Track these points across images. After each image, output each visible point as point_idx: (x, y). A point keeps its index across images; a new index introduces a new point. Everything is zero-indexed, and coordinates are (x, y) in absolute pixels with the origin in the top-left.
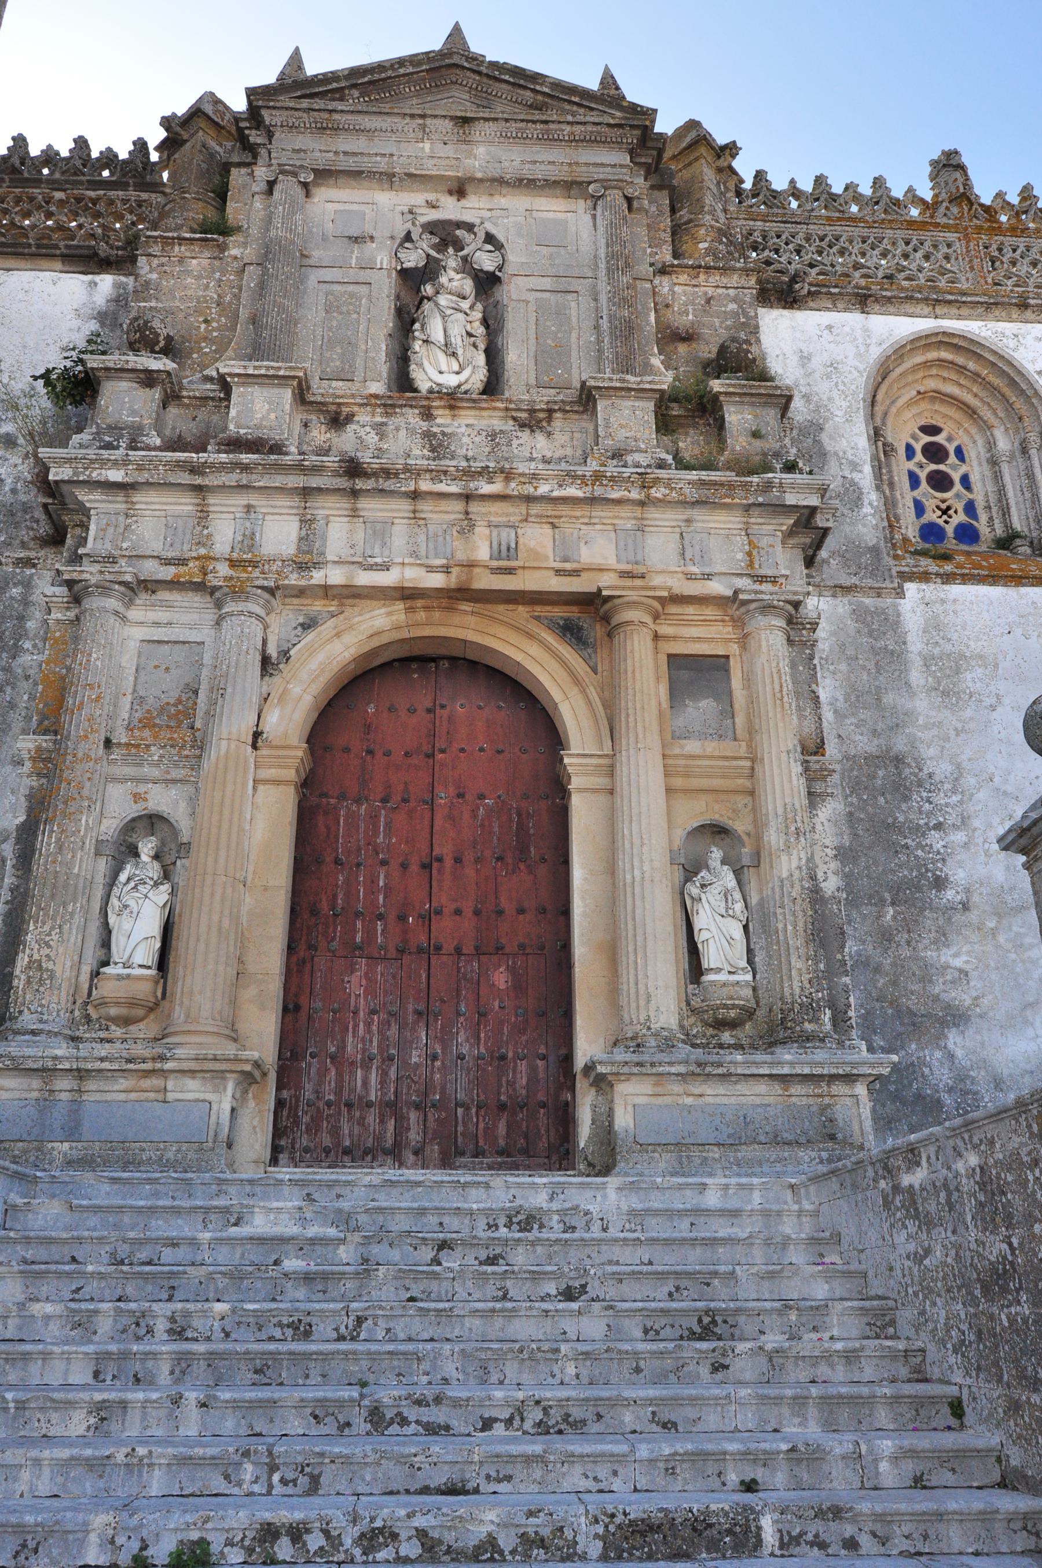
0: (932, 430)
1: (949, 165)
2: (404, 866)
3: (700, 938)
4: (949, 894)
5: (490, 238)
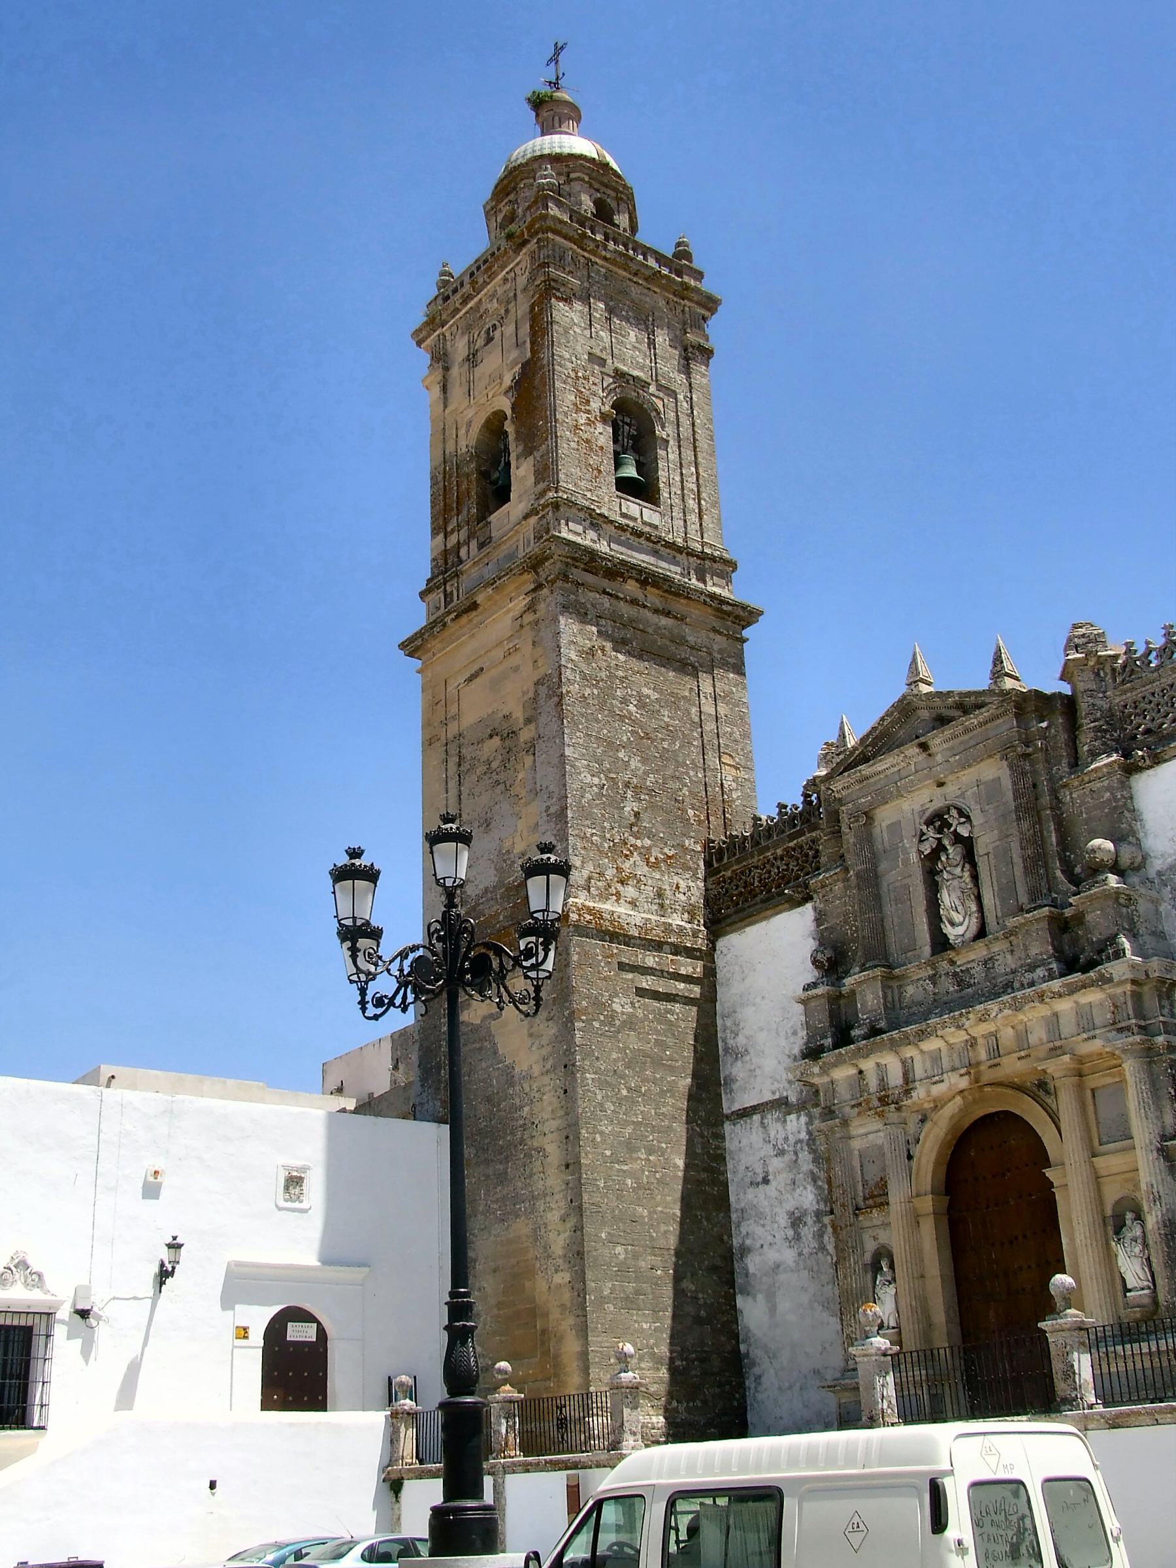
2: (1002, 1244)
3: (899, 1305)
5: (961, 813)
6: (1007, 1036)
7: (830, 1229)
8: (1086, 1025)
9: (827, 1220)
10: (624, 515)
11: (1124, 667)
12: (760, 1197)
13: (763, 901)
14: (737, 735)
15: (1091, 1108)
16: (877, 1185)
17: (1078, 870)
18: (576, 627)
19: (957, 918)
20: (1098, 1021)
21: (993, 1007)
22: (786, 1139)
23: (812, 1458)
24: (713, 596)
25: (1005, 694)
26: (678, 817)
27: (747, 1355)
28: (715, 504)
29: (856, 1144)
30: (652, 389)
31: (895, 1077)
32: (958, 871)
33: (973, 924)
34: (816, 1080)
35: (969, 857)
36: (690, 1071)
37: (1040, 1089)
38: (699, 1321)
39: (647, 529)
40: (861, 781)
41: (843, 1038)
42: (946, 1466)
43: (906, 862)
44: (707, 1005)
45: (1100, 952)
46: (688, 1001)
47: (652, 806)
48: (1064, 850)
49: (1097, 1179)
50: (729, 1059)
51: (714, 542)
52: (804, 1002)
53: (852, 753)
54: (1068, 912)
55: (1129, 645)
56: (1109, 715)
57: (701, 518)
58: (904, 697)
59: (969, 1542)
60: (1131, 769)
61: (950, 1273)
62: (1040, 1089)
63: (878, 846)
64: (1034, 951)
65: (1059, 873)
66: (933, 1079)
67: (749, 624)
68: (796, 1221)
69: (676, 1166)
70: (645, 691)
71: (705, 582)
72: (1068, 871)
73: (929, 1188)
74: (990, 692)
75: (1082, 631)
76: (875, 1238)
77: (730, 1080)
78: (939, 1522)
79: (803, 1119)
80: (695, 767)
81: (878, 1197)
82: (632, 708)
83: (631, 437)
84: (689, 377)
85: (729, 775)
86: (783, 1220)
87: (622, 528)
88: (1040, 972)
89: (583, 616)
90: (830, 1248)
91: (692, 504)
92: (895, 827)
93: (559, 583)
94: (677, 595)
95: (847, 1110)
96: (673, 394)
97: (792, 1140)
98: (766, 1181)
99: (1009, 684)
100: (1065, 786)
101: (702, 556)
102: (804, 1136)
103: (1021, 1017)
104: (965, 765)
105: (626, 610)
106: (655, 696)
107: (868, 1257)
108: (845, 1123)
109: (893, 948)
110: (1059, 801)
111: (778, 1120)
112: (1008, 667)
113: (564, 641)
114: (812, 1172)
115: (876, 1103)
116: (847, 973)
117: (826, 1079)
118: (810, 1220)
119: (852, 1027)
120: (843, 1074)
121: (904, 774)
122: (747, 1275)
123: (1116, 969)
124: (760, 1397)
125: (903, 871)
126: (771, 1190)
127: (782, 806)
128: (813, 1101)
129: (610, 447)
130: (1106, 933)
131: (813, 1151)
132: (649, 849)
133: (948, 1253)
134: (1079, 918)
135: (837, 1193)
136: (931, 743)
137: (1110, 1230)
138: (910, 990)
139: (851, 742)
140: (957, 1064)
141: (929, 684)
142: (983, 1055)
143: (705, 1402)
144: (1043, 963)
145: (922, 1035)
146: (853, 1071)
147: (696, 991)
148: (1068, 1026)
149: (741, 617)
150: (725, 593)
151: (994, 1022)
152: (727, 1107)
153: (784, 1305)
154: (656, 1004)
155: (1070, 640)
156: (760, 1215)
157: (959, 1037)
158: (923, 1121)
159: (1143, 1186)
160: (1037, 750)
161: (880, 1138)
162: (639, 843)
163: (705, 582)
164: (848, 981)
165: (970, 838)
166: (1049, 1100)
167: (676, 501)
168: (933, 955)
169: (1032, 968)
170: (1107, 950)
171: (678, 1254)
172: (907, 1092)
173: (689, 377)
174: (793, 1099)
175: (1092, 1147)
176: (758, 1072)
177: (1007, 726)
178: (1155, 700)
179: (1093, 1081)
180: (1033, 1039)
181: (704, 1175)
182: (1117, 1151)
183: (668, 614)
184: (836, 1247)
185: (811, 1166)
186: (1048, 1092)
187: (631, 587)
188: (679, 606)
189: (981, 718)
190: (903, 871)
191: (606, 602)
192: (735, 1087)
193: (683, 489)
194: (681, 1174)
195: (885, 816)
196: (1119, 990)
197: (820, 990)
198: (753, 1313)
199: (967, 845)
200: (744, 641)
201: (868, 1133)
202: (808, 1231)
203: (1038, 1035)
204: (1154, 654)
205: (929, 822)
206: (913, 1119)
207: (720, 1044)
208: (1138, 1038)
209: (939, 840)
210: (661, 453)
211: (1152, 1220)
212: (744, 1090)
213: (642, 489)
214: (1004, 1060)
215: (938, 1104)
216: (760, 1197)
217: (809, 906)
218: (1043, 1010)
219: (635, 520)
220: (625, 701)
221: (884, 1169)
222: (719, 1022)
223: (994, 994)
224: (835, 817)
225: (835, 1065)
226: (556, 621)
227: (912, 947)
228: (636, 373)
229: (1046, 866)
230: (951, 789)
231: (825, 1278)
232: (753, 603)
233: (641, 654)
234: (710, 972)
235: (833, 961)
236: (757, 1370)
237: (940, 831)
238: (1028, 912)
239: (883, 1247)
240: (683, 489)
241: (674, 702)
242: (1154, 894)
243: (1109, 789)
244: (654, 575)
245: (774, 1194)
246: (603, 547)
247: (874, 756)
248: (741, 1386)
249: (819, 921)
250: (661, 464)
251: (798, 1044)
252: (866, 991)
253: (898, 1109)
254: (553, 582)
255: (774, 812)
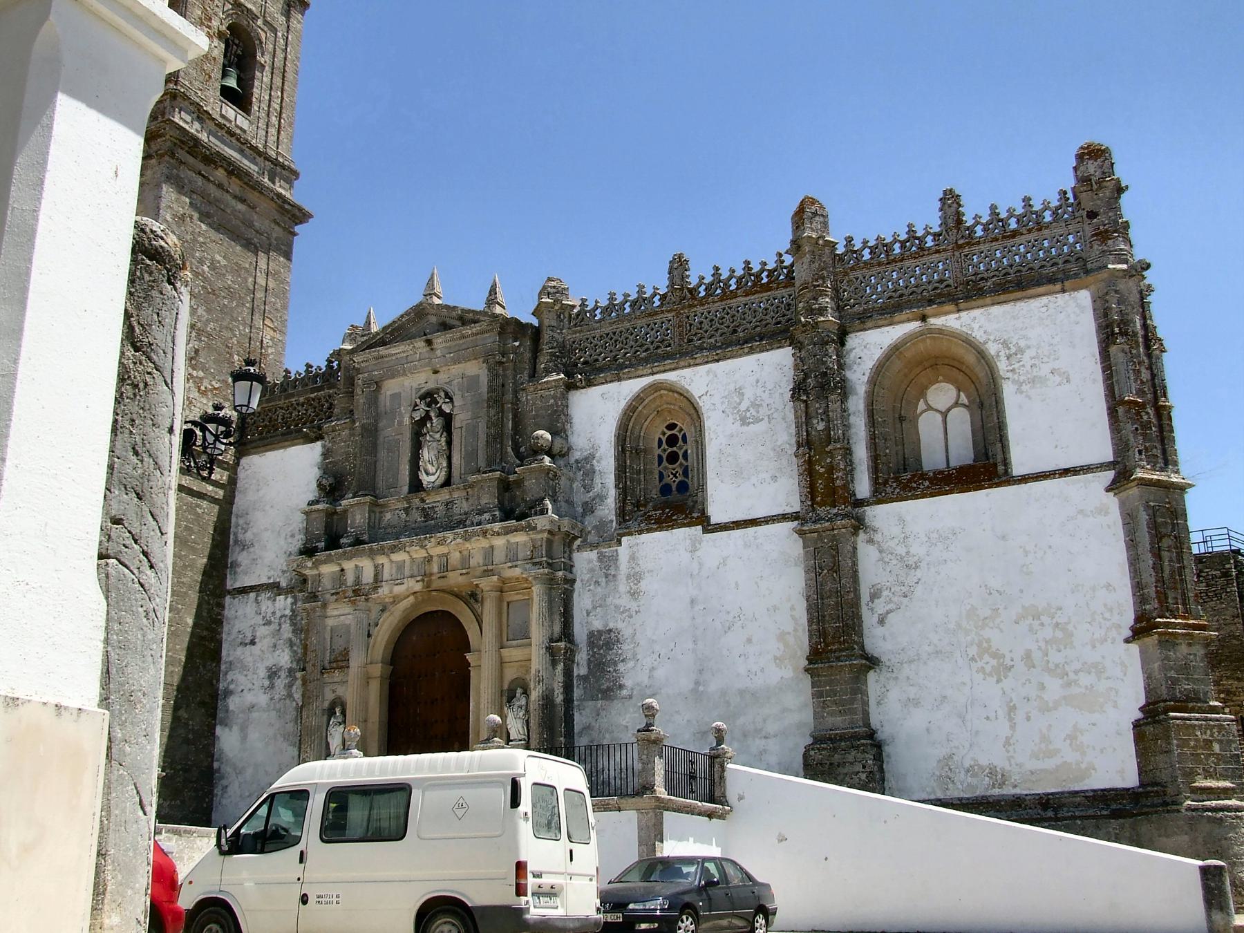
0: (672, 427)
1: (950, 200)
4: (624, 692)
5: (447, 396)
6: (455, 557)
7: (299, 682)
8: (512, 557)
9: (299, 675)
10: (222, 116)
11: (578, 314)
12: (247, 655)
13: (283, 434)
14: (278, 306)
15: (505, 615)
16: (340, 654)
17: (522, 449)
18: (174, 196)
19: (431, 469)
20: (521, 556)
21: (449, 535)
22: (274, 613)
23: (432, 767)
24: (279, 195)
25: (495, 317)
26: (226, 359)
27: (219, 770)
28: (291, 125)
29: (330, 622)
30: (260, 22)
31: (368, 577)
32: (437, 436)
33: (443, 475)
34: (307, 572)
35: (448, 427)
36: (207, 553)
37: (472, 597)
38: (187, 741)
39: (238, 131)
40: (377, 359)
41: (333, 542)
42: (522, 771)
43: (400, 423)
44: (226, 506)
45: (531, 508)
46: (214, 500)
47: (209, 347)
48: (516, 434)
49: (502, 663)
50: (238, 549)
51: (287, 153)
52: (306, 513)
53: (374, 336)
54: (512, 478)
55: (583, 300)
56: (562, 346)
57: (279, 132)
58: (421, 304)
59: (530, 815)
60: (571, 386)
61: (386, 720)
62: (472, 597)
63: (382, 409)
64: (484, 501)
65: (509, 450)
66: (395, 581)
67: (301, 223)
68: (273, 674)
69: (186, 624)
70: (218, 257)
71: (274, 183)
72: (516, 449)
73: (380, 658)
74: (484, 313)
75: (554, 284)
76: (334, 691)
77: (235, 565)
78: (515, 802)
79: (290, 600)
80: (245, 325)
81: (341, 661)
82: (205, 268)
83: (237, 56)
84: (288, 20)
85: (268, 335)
86: (262, 673)
87: (220, 126)
88: (486, 516)
89: (180, 187)
90: (298, 696)
91: (274, 120)
92: (396, 397)
93: (167, 158)
94: (253, 188)
95: (328, 596)
96: (275, 31)
97: (278, 614)
98: (253, 643)
99: (498, 310)
100: (523, 390)
101: (275, 163)
102: (288, 612)
103: (468, 545)
104: (456, 361)
105: (214, 191)
106: (224, 262)
107: (326, 705)
108: (325, 606)
109: (381, 484)
110: (518, 400)
111: (269, 598)
112: (499, 298)
113: (163, 205)
114: (290, 640)
115: (350, 594)
116: (342, 497)
117: (315, 572)
118: (283, 674)
119: (342, 537)
120: (328, 569)
121: (410, 359)
122: (227, 711)
123: (540, 522)
124: (224, 802)
125: (398, 429)
126: (255, 650)
127: (309, 366)
128: (301, 586)
129: (221, 59)
130: (537, 496)
131: (293, 624)
132: (201, 379)
133: (386, 708)
134: (519, 483)
135: (311, 655)
136: (435, 341)
137: (505, 699)
138: (388, 516)
139: (375, 328)
140: (416, 573)
141: (439, 298)
142: (435, 569)
143: (183, 802)
144: (489, 510)
145: (394, 549)
146: (337, 569)
147: (220, 494)
148: (499, 556)
149: (295, 215)
150: (288, 195)
151: (449, 547)
152: (230, 584)
153: (254, 735)
154: (190, 499)
155: (544, 288)
156: (244, 668)
157: (420, 554)
158: (383, 611)
159: (533, 671)
160: (509, 360)
161: (349, 620)
162: (195, 373)
163: (274, 183)
164: (344, 503)
165: (450, 414)
166: (476, 606)
167: (263, 115)
168: (410, 492)
169: (481, 512)
170: (536, 508)
171: (179, 689)
172: (376, 589)
173: (288, 20)
174: (284, 584)
175: (501, 643)
176: (259, 561)
177: (490, 340)
178: (595, 342)
179: (513, 596)
180: (473, 562)
181: (205, 633)
182: (518, 646)
183: (243, 201)
184: (303, 696)
185: (290, 635)
186: (477, 601)
187: (220, 174)
188: (253, 196)
189: (474, 330)
190: (398, 429)
191: (200, 180)
192: (239, 570)
193: (269, 106)
194: (189, 630)
195: (391, 387)
196: (539, 536)
197: (321, 506)
198: (228, 740)
199: (448, 419)
200: (294, 234)
201: (340, 615)
202: (280, 683)
203: (477, 560)
204: (599, 310)
205: (422, 398)
206: (376, 609)
207: (232, 537)
208: (546, 570)
209: (427, 412)
210: (258, 74)
211: (535, 695)
212: (246, 573)
213: (239, 98)
214: (450, 574)
215: (396, 600)
216: (247, 655)
217: (319, 443)
218: (484, 543)
219: (230, 122)
220: (201, 261)
221: (348, 642)
222: (233, 520)
223: (450, 527)
224: (351, 382)
225: (325, 562)
226: (159, 186)
227: (393, 485)
228: (250, 6)
229: (502, 443)
230: (443, 377)
231: (288, 717)
232: (307, 207)
233: (219, 227)
234: (233, 481)
235: (333, 486)
236: (224, 782)
237: (429, 405)
238: (485, 472)
239: (339, 698)
240: (269, 106)
241: (237, 270)
242: (571, 474)
243: (554, 397)
244: (239, 168)
245: (258, 653)
246: (203, 137)
247: (390, 342)
248: (210, 794)
249: (325, 455)
250: (257, 83)
251: (297, 542)
252: (355, 509)
253: (367, 600)
254: (162, 156)
255: (302, 370)
